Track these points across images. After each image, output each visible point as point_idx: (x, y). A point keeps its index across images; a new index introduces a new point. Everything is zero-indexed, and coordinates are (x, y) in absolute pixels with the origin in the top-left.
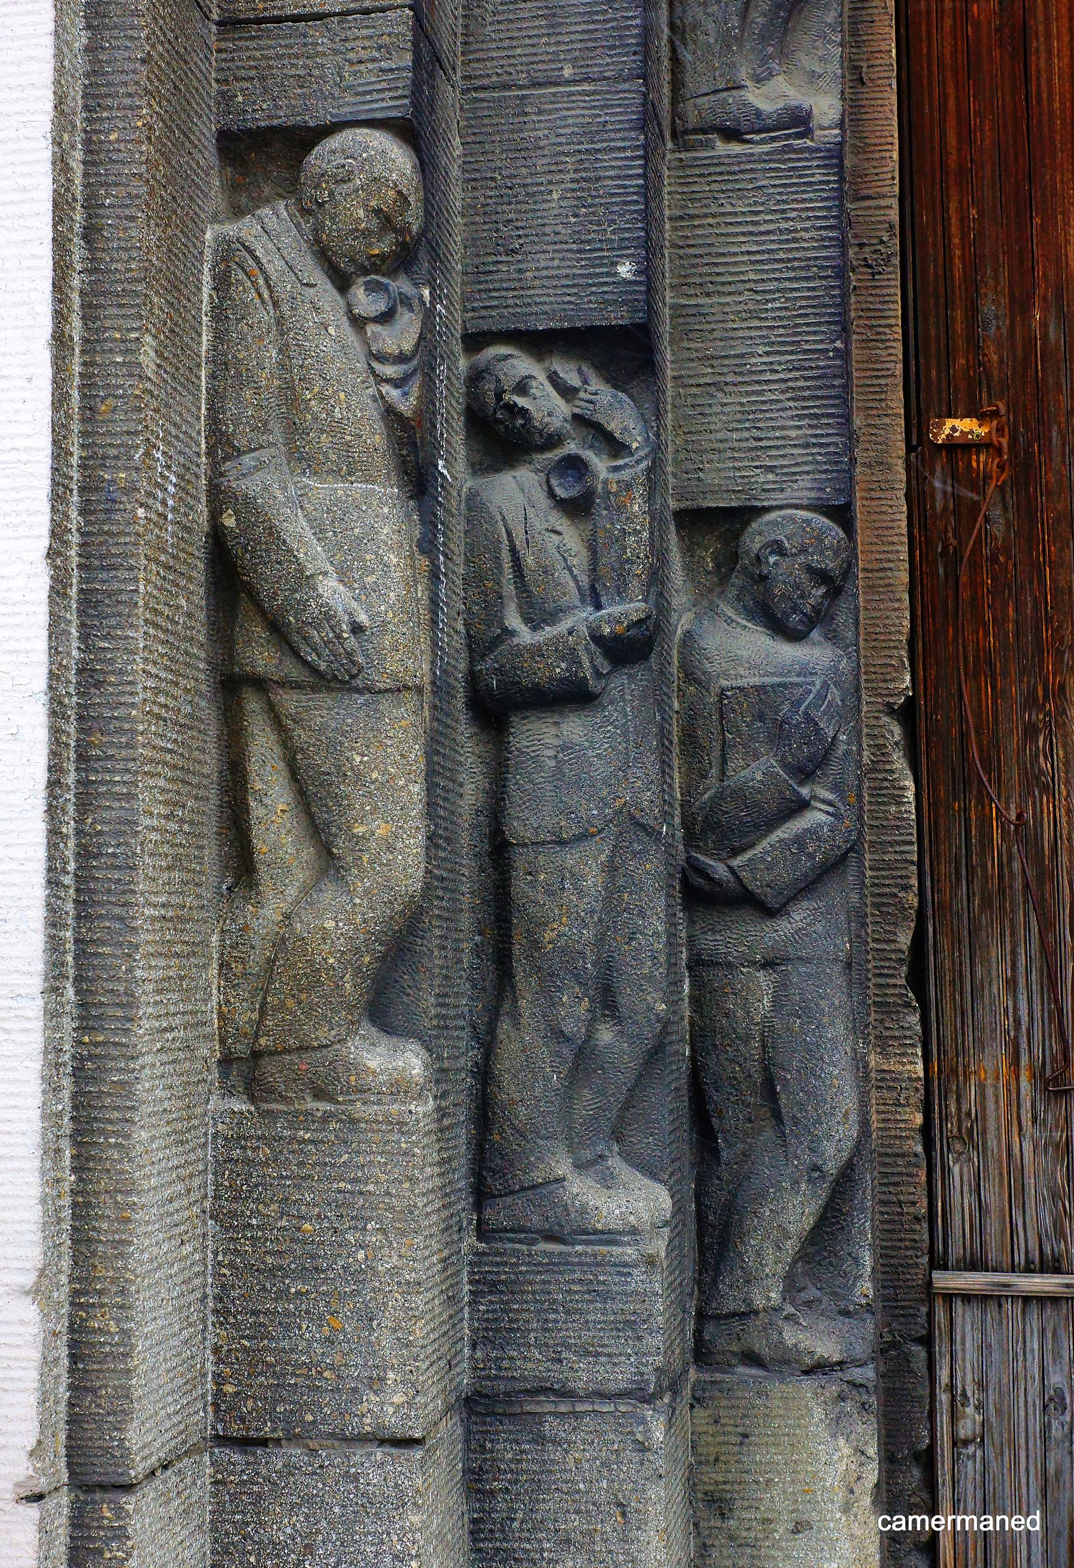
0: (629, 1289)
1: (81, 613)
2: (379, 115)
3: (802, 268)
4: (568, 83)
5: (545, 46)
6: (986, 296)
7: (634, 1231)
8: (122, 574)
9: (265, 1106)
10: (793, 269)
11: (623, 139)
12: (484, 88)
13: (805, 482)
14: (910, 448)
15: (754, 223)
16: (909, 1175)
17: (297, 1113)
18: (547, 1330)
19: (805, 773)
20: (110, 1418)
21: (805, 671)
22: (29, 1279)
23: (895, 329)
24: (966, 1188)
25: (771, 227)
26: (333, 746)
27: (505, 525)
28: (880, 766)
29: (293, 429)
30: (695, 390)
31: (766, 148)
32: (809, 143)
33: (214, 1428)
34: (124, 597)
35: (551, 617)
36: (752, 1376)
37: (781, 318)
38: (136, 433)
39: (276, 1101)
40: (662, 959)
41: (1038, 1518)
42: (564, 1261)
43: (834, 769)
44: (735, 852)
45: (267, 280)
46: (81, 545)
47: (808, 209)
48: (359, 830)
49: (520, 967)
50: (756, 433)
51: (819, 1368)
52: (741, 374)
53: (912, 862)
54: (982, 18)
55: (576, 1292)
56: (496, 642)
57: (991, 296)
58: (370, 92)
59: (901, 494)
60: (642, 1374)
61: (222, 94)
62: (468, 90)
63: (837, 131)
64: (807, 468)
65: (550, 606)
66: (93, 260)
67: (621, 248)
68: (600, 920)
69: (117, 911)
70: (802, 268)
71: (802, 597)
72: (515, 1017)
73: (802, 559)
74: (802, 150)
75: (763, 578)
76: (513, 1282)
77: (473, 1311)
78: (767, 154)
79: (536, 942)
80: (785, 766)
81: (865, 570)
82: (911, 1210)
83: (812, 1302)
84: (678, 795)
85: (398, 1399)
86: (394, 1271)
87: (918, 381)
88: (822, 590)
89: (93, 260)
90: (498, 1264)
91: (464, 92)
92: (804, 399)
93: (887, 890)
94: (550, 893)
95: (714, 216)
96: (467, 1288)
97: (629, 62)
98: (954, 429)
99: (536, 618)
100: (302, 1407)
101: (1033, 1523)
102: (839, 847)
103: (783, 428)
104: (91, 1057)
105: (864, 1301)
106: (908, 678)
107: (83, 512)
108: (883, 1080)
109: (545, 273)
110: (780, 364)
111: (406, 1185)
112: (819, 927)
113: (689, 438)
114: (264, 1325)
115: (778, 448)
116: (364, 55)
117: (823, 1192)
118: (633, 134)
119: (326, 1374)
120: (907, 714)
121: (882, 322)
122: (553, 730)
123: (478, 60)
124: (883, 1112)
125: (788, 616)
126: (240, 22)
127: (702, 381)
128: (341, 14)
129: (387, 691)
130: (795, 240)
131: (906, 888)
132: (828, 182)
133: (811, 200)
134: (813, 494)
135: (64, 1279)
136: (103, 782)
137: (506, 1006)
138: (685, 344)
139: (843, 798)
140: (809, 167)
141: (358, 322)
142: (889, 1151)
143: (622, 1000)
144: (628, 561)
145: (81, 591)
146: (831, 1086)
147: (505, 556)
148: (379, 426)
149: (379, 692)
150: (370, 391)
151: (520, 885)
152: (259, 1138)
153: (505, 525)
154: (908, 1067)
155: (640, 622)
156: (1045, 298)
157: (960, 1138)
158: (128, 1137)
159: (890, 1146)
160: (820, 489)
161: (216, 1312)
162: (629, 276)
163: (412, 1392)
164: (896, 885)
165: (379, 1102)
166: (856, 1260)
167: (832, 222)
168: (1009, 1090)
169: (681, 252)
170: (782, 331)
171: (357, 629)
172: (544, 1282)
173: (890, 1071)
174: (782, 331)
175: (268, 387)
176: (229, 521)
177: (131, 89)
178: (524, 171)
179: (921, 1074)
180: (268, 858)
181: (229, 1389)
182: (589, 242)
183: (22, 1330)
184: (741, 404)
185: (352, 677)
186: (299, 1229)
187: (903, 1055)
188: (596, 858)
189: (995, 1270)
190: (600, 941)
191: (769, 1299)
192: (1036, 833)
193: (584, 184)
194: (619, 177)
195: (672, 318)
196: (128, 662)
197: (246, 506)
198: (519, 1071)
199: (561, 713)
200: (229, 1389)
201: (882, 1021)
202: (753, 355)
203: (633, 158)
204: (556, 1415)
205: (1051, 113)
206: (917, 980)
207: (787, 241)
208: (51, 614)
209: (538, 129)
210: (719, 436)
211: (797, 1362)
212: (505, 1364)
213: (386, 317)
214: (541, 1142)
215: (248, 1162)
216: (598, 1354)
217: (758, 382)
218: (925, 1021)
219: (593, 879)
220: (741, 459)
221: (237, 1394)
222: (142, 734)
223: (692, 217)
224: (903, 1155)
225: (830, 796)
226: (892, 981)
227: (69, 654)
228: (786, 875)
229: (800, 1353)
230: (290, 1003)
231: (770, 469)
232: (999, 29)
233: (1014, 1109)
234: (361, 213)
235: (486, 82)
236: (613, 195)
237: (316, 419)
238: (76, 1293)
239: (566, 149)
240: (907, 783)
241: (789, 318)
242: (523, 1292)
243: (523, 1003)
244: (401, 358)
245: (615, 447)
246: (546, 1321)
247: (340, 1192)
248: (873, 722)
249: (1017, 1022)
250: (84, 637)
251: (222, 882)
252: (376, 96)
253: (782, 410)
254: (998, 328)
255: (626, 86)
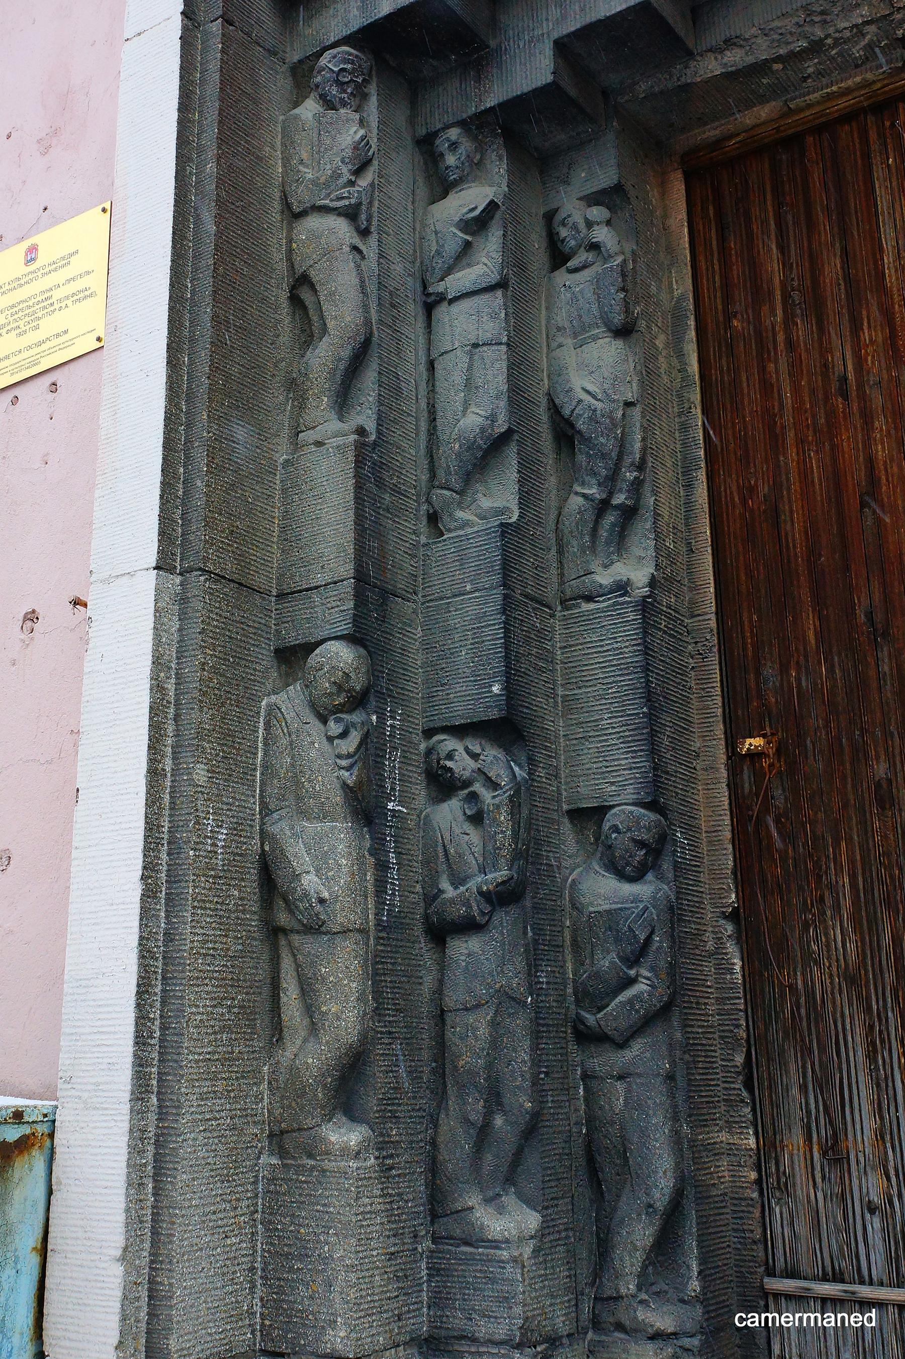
0: (505, 1277)
1: (167, 905)
2: (339, 634)
3: (625, 669)
4: (469, 593)
5: (458, 575)
6: (765, 664)
7: (507, 1241)
8: (183, 884)
9: (285, 1161)
10: (621, 669)
11: (494, 619)
12: (431, 600)
13: (630, 789)
14: (729, 758)
15: (602, 646)
16: (749, 1212)
17: (299, 1166)
18: (465, 1300)
19: (634, 960)
20: (164, 1332)
21: (636, 900)
22: (119, 1253)
23: (717, 689)
24: (785, 1222)
25: (609, 647)
26: (313, 964)
27: (441, 832)
28: (720, 951)
29: (299, 798)
30: (574, 742)
31: (606, 604)
32: (627, 599)
33: (260, 1345)
34: (183, 896)
35: (463, 881)
36: (620, 1339)
37: (616, 697)
38: (191, 814)
39: (289, 1159)
40: (528, 1076)
41: (873, 1315)
42: (472, 1258)
43: (651, 956)
44: (600, 1009)
45: (286, 723)
46: (168, 871)
47: (626, 636)
48: (324, 1009)
49: (450, 1081)
50: (605, 763)
51: (657, 1336)
52: (597, 731)
53: (741, 1010)
54: (755, 506)
55: (479, 1277)
56: (435, 897)
57: (769, 664)
58: (335, 623)
59: (724, 785)
60: (512, 1331)
61: (276, 630)
62: (424, 603)
63: (647, 589)
64: (631, 782)
65: (462, 875)
66: (177, 730)
67: (494, 677)
68: (488, 1054)
69: (175, 1057)
70: (625, 669)
71: (630, 857)
72: (447, 1109)
73: (629, 835)
74: (623, 603)
75: (610, 847)
76: (448, 1269)
77: (428, 1286)
78: (606, 607)
79: (456, 1067)
80: (619, 957)
81: (706, 832)
82: (751, 1235)
83: (659, 1292)
84: (571, 976)
85: (342, 1334)
86: (342, 1259)
87: (730, 717)
88: (644, 852)
89: (177, 730)
90: (440, 1258)
91: (423, 604)
92: (629, 742)
93: (727, 1028)
94: (461, 1038)
95: (581, 644)
96: (426, 1271)
97: (497, 578)
98: (751, 745)
99: (457, 881)
100: (299, 1335)
101: (870, 1319)
102: (655, 1006)
103: (618, 759)
104: (163, 1134)
105: (693, 1294)
106: (733, 896)
107: (169, 854)
108: (731, 1149)
109: (459, 694)
110: (616, 723)
111: (348, 1209)
112: (648, 1055)
113: (572, 768)
114: (281, 1286)
115: (616, 771)
116: (334, 604)
117: (657, 1222)
118: (499, 616)
119: (310, 1317)
120: (734, 916)
121: (710, 685)
122: (465, 945)
123: (429, 587)
124: (732, 1171)
125: (625, 868)
126: (285, 594)
127: (578, 736)
128: (325, 585)
129: (339, 933)
130: (621, 653)
131: (738, 1026)
132: (637, 619)
133: (629, 630)
134: (635, 797)
135: (145, 1254)
136: (172, 990)
137: (443, 1106)
138: (570, 717)
139: (657, 976)
140: (627, 612)
141: (330, 739)
142: (736, 1196)
143: (505, 1101)
144: (497, 848)
145: (166, 894)
146: (656, 1154)
147: (440, 849)
148: (339, 792)
149: (335, 933)
150: (336, 774)
151: (448, 1035)
152: (282, 1179)
153: (441, 832)
154: (745, 1142)
155: (504, 882)
156: (798, 662)
157: (779, 1188)
158: (175, 1178)
159: (736, 1193)
160: (638, 793)
161: (261, 1277)
162: (497, 692)
163: (349, 1330)
164: (733, 1025)
165: (335, 1161)
166: (688, 1266)
167: (639, 641)
168: (805, 1158)
169: (566, 666)
170: (616, 705)
171: (322, 901)
172: (463, 1270)
173: (734, 1144)
174: (616, 705)
175: (284, 778)
176: (267, 848)
177: (194, 647)
178: (449, 642)
179: (754, 1146)
180: (289, 1023)
181: (267, 1323)
182: (479, 675)
183: (114, 1280)
184: (598, 748)
185: (320, 926)
186: (299, 1232)
187: (741, 1133)
188: (485, 1018)
189: (805, 1279)
190: (489, 1066)
191: (628, 1289)
192: (812, 987)
193: (477, 645)
194: (493, 640)
195: (562, 702)
196: (184, 929)
197: (273, 839)
198: (448, 1142)
199: (469, 935)
200: (267, 1323)
201: (728, 1111)
202: (602, 719)
203: (499, 629)
204: (471, 1353)
205: (796, 554)
206: (748, 1085)
207: (618, 654)
208: (142, 908)
209: (455, 620)
210: (587, 766)
211: (644, 1331)
212: (444, 1319)
213: (344, 735)
214: (460, 1185)
215: (277, 1193)
216: (490, 1317)
217: (606, 735)
218: (754, 1110)
219: (483, 1031)
220: (598, 779)
221: (271, 1325)
222: (189, 965)
223: (571, 646)
224: (745, 1199)
225: (649, 975)
226: (733, 1086)
227: (159, 927)
228: (623, 1024)
229: (646, 1325)
230: (293, 1104)
231: (612, 783)
232: (765, 511)
233: (809, 1170)
234: (327, 685)
235: (432, 597)
236: (490, 649)
237: (307, 791)
238: (152, 1262)
239: (467, 628)
240: (735, 961)
241: (620, 697)
242: (453, 1276)
243: (450, 1103)
244: (349, 756)
245: (493, 785)
246: (464, 1294)
247: (318, 1211)
248: (714, 923)
249: (809, 1112)
250: (167, 917)
251: (273, 1036)
252: (339, 624)
253: (618, 749)
254: (774, 682)
255: (495, 591)
